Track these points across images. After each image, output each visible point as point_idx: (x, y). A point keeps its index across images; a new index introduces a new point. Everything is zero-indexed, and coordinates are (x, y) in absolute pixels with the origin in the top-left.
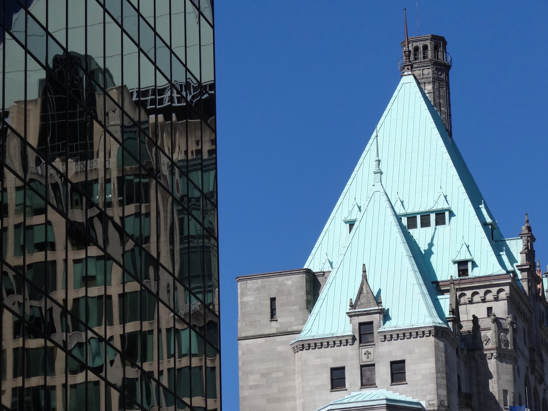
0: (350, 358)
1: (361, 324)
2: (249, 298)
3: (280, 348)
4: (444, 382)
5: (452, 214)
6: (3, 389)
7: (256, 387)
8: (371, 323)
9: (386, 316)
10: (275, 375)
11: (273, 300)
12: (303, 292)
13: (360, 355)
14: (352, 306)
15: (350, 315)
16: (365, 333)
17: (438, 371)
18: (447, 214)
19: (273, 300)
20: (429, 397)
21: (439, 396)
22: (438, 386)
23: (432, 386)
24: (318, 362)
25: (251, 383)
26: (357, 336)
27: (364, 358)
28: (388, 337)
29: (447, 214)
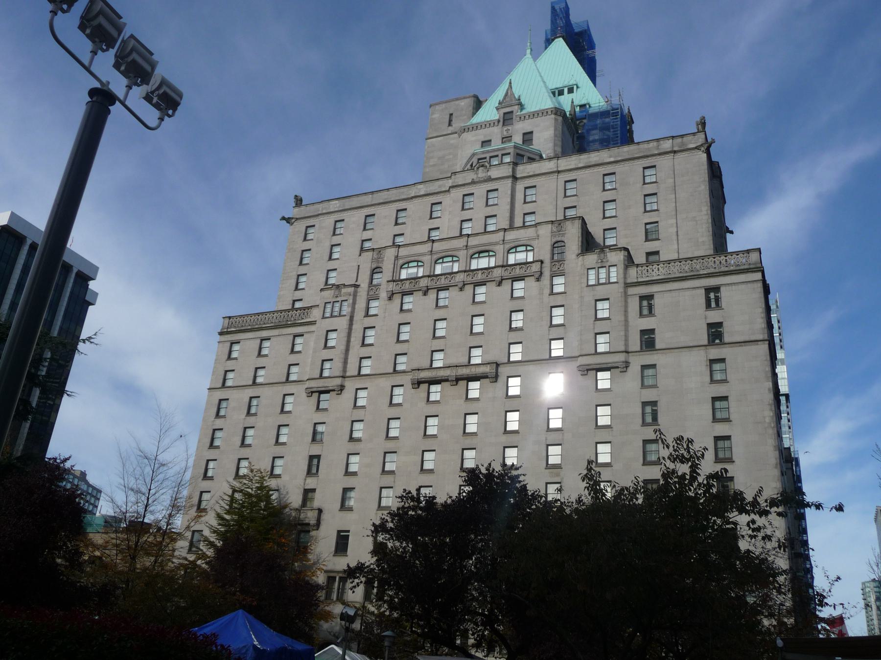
0: (495, 134)
1: (505, 114)
2: (436, 116)
3: (452, 142)
4: (560, 143)
5: (578, 87)
6: (571, 491)
7: (434, 165)
8: (512, 112)
9: (521, 106)
10: (447, 157)
11: (451, 115)
12: (471, 108)
13: (502, 132)
14: (500, 103)
15: (497, 109)
16: (507, 119)
17: (555, 136)
18: (575, 87)
19: (451, 115)
20: (548, 152)
21: (555, 151)
22: (555, 145)
23: (551, 145)
24: (474, 139)
25: (431, 164)
26: (502, 120)
27: (505, 133)
28: (522, 118)
29: (575, 87)
